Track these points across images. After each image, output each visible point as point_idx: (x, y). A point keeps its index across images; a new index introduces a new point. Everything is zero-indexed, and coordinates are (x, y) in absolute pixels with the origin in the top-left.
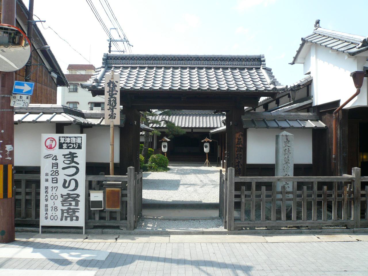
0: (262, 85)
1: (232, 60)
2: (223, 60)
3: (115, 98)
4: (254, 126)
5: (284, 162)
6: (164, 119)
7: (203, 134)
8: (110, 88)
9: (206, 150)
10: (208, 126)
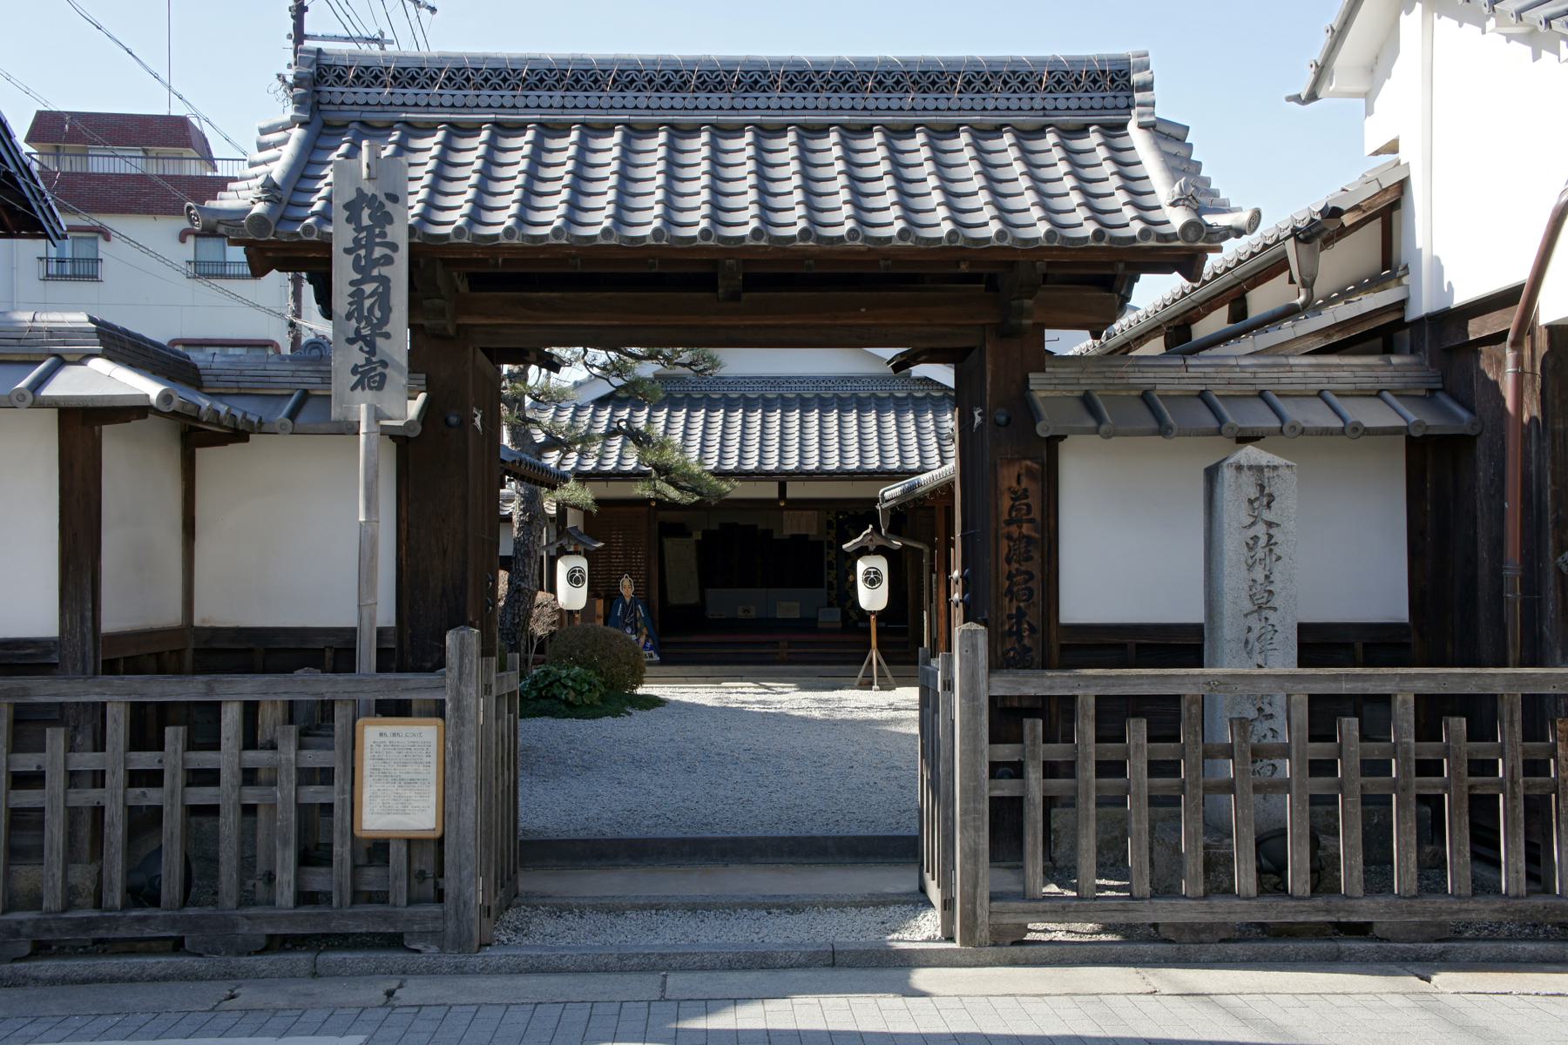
0: (1129, 212)
1: (978, 84)
2: (934, 83)
3: (384, 281)
4: (1091, 423)
5: (1248, 606)
6: (623, 424)
7: (846, 512)
8: (359, 229)
9: (872, 598)
10: (873, 463)
